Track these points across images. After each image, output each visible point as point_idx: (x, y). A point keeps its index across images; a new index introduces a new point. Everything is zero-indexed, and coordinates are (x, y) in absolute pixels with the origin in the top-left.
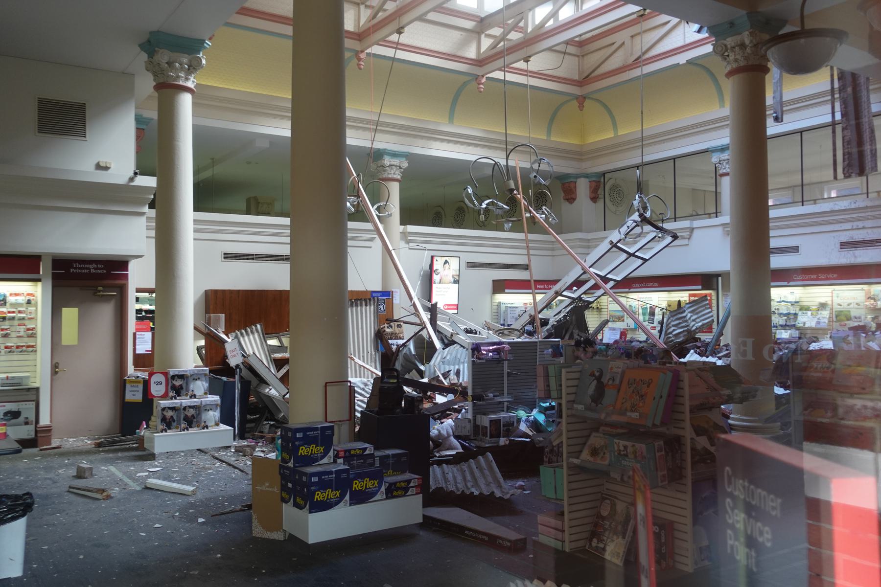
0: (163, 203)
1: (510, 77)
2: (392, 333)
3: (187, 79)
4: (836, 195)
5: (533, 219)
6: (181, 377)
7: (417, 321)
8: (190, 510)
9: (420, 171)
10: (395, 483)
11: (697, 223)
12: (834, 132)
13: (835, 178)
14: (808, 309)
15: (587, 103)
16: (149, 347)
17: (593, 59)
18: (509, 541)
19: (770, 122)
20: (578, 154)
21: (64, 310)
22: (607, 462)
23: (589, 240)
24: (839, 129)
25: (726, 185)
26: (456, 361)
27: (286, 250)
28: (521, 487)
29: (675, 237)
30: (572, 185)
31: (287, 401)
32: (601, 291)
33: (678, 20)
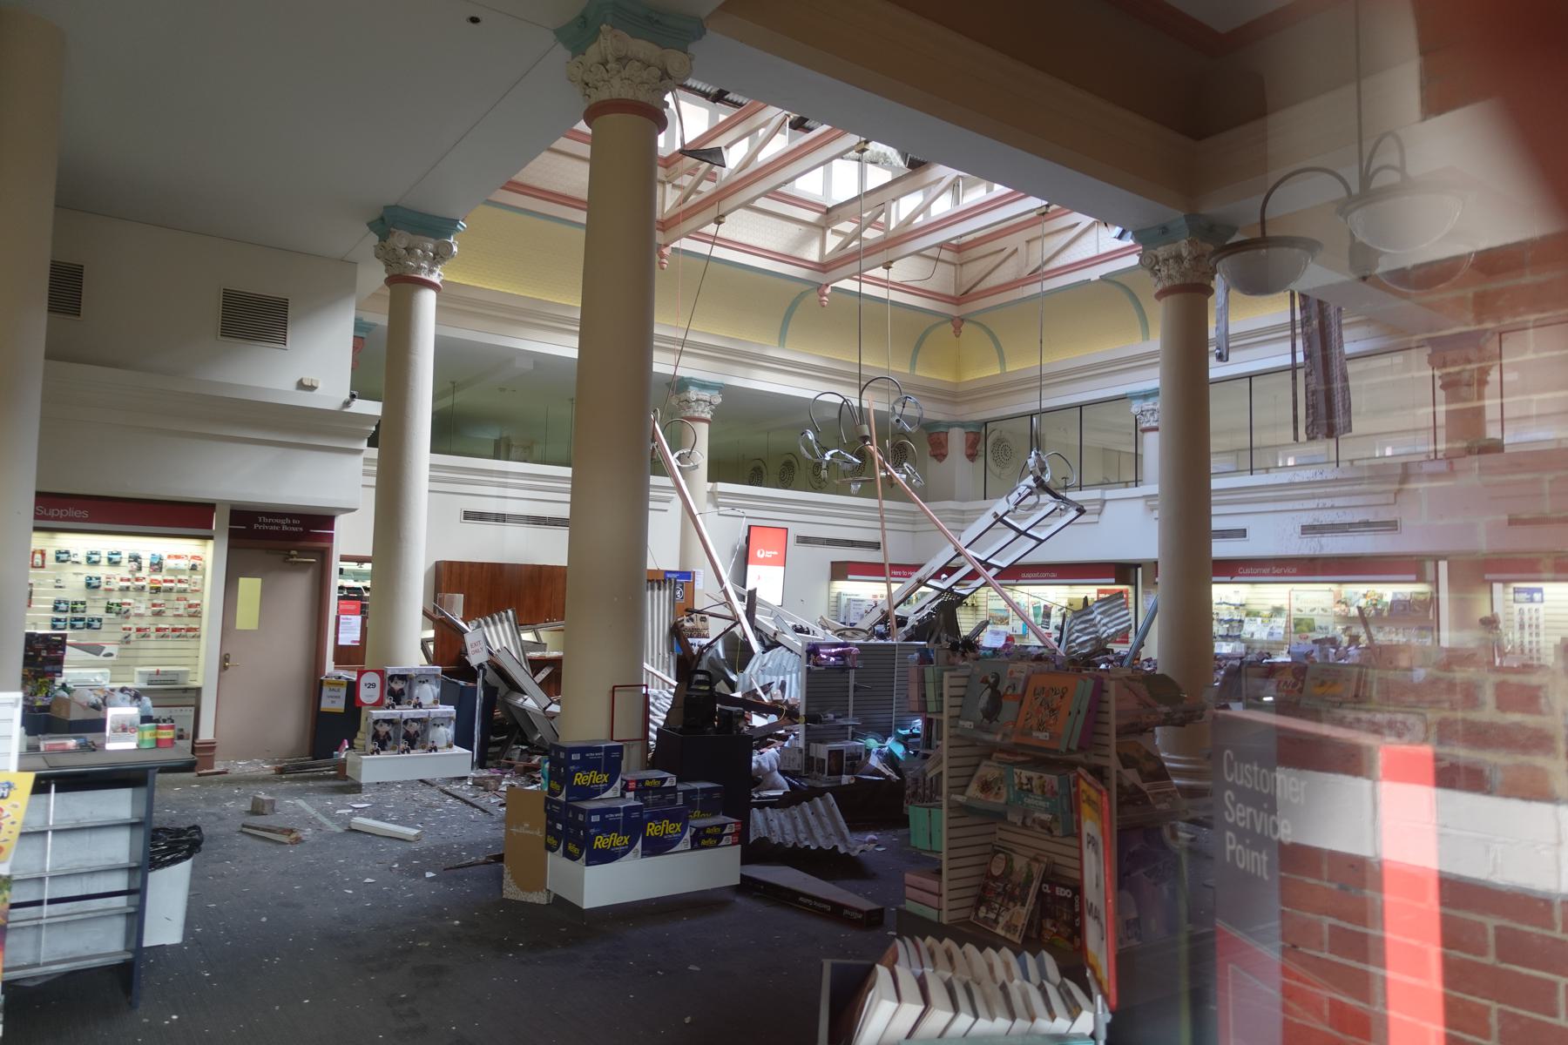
0: (388, 439)
1: (868, 289)
2: (693, 629)
3: (431, 271)
4: (1297, 462)
5: (890, 480)
6: (403, 678)
7: (729, 614)
8: (413, 862)
9: (738, 411)
10: (704, 829)
11: (1110, 494)
12: (1294, 378)
13: (1296, 438)
14: (1257, 614)
15: (965, 327)
16: (357, 636)
17: (974, 271)
18: (860, 911)
19: (1212, 360)
20: (952, 396)
21: (242, 581)
22: (1002, 801)
23: (963, 512)
24: (1301, 374)
25: (1152, 447)
26: (780, 670)
27: (564, 511)
28: (873, 841)
29: (1081, 511)
30: (942, 437)
31: (553, 716)
32: (981, 581)
33: (1092, 220)
